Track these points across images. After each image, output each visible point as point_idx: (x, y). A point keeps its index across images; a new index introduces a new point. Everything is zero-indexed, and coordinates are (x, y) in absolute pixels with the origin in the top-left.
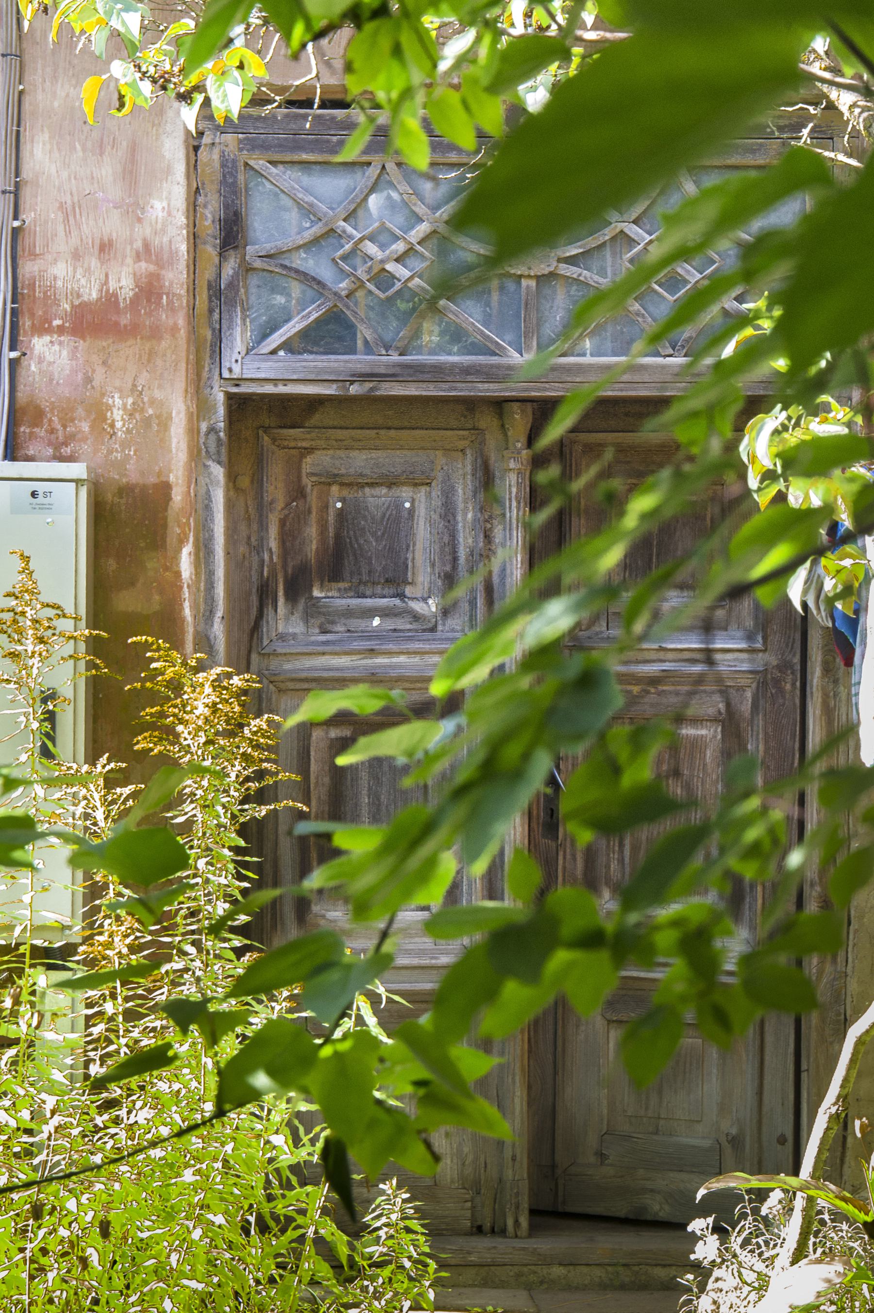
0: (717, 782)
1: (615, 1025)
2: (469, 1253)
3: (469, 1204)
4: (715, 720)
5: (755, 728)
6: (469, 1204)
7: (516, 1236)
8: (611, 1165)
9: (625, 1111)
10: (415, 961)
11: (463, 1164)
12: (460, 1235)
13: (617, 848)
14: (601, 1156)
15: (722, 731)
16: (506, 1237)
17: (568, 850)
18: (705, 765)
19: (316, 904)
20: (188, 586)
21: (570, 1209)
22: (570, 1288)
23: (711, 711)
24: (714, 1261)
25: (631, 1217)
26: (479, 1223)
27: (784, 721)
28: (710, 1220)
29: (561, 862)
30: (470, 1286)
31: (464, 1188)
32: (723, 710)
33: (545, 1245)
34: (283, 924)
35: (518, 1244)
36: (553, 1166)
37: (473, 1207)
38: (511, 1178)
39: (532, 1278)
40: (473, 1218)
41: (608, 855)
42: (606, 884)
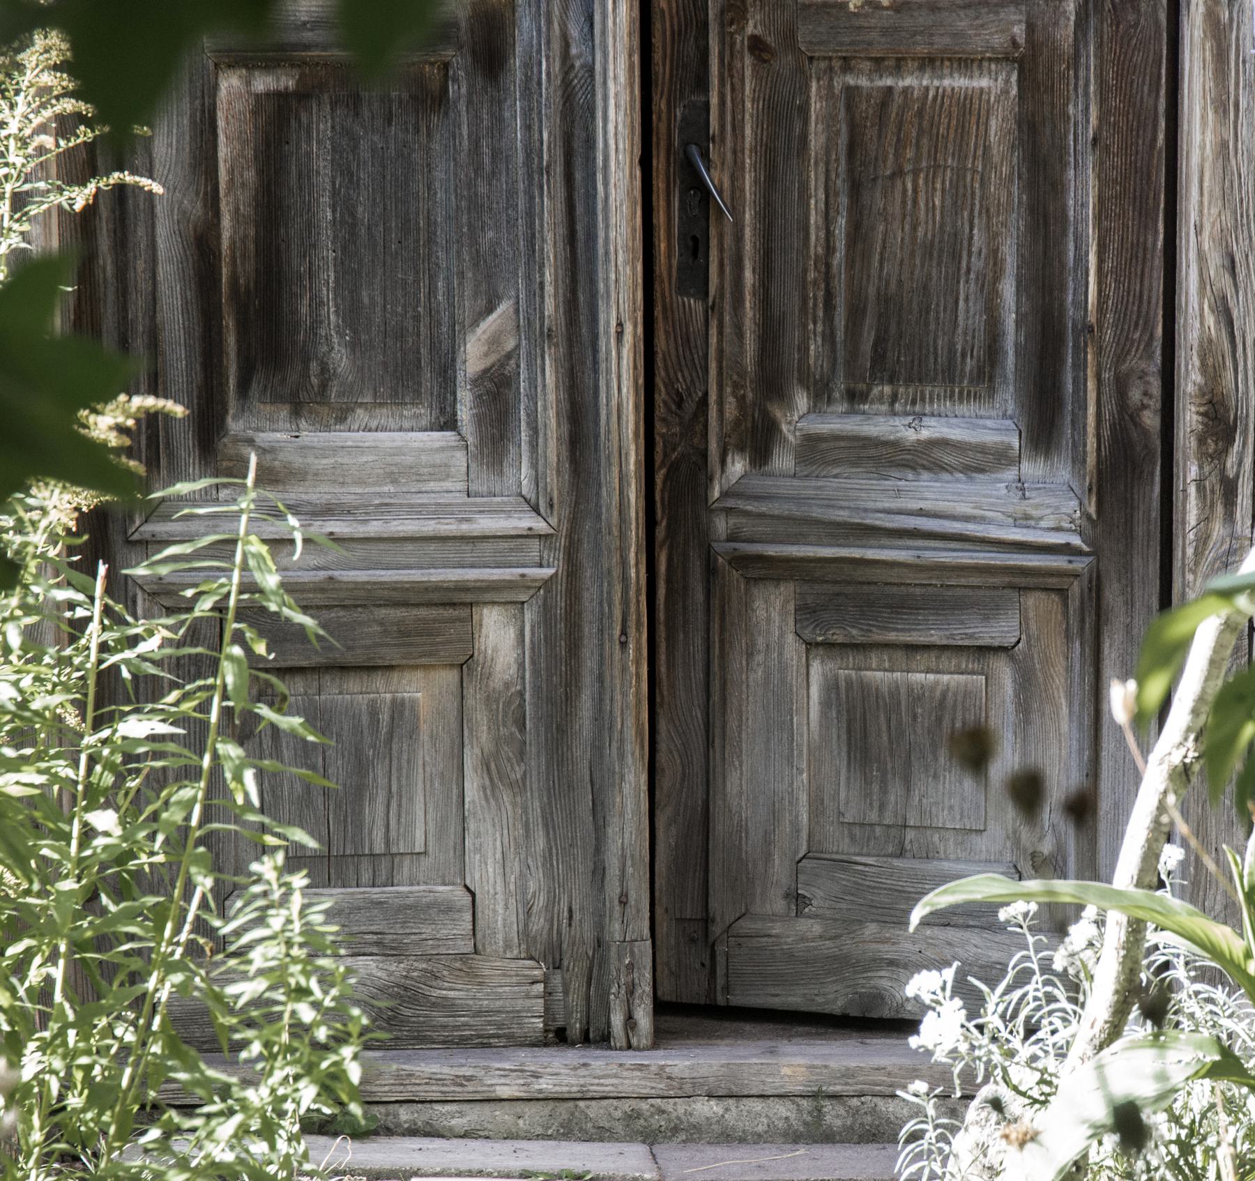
0: (1011, 181)
1: (821, 651)
2: (536, 1076)
3: (540, 988)
4: (1005, 58)
5: (1082, 74)
6: (540, 988)
7: (629, 1047)
8: (816, 916)
9: (841, 814)
10: (429, 527)
11: (528, 913)
12: (522, 1045)
13: (821, 314)
14: (798, 901)
15: (1019, 81)
16: (610, 1048)
17: (727, 318)
18: (987, 148)
19: (235, 417)
20: (1231, 781)
21: (737, 1000)
22: (727, 1137)
23: (998, 40)
24: (955, 1050)
25: (854, 1012)
26: (560, 1023)
27: (1138, 58)
28: (949, 974)
29: (713, 340)
30: (538, 1137)
31: (532, 958)
32: (1021, 40)
33: (683, 1061)
34: (171, 456)
35: (630, 1058)
36: (706, 920)
37: (548, 994)
38: (617, 937)
39: (658, 1121)
40: (548, 1013)
41: (805, 326)
42: (800, 381)
